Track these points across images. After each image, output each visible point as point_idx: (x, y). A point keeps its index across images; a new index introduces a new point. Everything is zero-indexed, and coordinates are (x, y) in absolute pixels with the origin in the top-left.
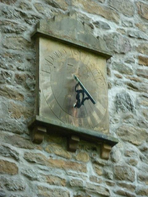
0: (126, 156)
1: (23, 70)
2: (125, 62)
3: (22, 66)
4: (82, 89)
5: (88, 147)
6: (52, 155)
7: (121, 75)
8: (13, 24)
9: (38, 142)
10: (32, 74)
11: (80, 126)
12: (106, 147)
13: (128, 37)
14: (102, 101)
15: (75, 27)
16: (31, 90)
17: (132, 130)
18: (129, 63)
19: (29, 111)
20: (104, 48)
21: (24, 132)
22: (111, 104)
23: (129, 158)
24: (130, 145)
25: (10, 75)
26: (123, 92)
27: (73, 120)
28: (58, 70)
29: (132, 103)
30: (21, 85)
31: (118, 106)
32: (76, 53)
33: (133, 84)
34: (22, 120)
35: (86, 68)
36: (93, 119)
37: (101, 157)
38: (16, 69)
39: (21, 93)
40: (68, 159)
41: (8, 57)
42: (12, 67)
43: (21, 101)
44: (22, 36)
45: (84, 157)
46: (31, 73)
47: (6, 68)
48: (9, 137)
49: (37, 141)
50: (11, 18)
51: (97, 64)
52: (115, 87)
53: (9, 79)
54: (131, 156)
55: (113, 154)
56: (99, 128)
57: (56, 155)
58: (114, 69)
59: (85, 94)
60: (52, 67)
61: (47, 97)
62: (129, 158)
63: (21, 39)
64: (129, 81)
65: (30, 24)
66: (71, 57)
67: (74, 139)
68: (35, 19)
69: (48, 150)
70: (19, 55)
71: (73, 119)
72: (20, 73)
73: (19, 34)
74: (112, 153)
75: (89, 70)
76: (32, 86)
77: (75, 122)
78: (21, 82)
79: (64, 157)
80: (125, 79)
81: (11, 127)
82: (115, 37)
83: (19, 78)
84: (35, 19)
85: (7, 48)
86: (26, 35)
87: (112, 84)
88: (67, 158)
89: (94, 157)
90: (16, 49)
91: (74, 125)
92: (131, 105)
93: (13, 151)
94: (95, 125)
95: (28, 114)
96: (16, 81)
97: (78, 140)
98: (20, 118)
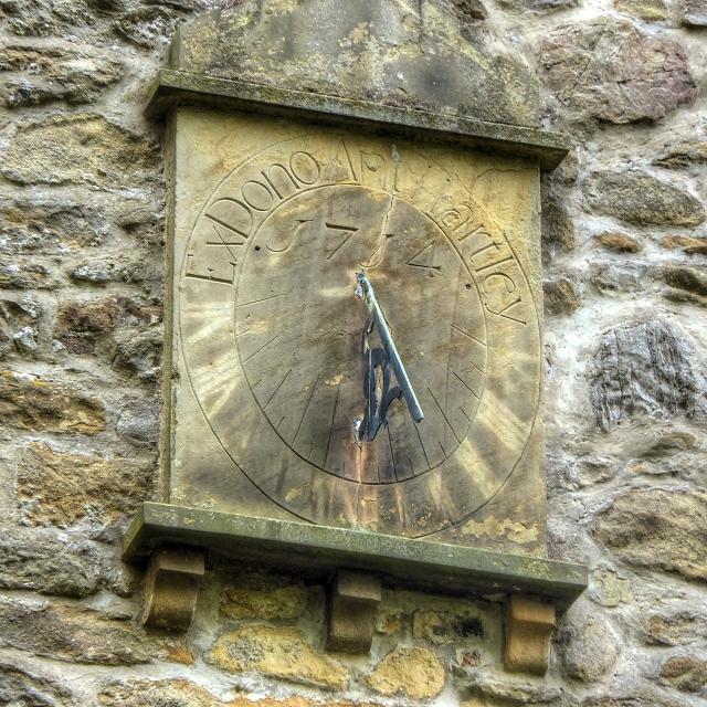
0: (648, 644)
1: (99, 284)
2: (658, 164)
3: (96, 261)
4: (382, 347)
5: (435, 621)
6: (247, 681)
7: (631, 234)
8: (50, 61)
9: (170, 628)
10: (148, 292)
11: (389, 522)
12: (525, 613)
13: (675, 34)
14: (509, 387)
15: (371, 32)
16: (140, 375)
17: (682, 512)
18: (676, 167)
19: (126, 476)
20: (529, 110)
21: (103, 584)
22: (567, 396)
23: (664, 655)
24: (672, 584)
25: (29, 314)
26: (639, 320)
27: (347, 500)
28: (274, 260)
29: (684, 374)
30: (95, 356)
31: (611, 394)
32: (373, 161)
33: (694, 271)
34: (89, 527)
35: (428, 227)
36: (459, 485)
37: (511, 668)
38: (66, 282)
39: (87, 394)
40: (333, 691)
41: (23, 228)
42: (44, 273)
43: (89, 435)
44: (98, 110)
45: (418, 672)
46: (140, 293)
47: (16, 286)
48: (22, 619)
49: (164, 622)
50: (37, 30)
51: (487, 200)
52: (597, 298)
53: (24, 332)
54: (672, 641)
55: (574, 642)
56: (489, 520)
57: (270, 677)
58: (593, 207)
59: (393, 377)
60: (243, 253)
61: (211, 400)
62: (664, 655)
63: (93, 128)
64: (671, 258)
65: (145, 47)
66: (349, 184)
67: (353, 591)
68: (162, 13)
69: (224, 657)
70: (75, 211)
71: (352, 491)
72: (85, 297)
73: (85, 102)
74: (563, 641)
75: (433, 234)
76: (144, 353)
77: (358, 508)
78: (90, 340)
79: (310, 686)
80: (657, 254)
81: (31, 568)
82: (604, 41)
83: (77, 322)
84: (166, 17)
85: (21, 184)
86: (122, 109)
87: (581, 288)
88: (328, 689)
89: (470, 670)
90: (65, 183)
91: (357, 523)
92: (679, 382)
93: (41, 682)
94: (466, 508)
95: (124, 492)
96: (62, 338)
97: (374, 595)
98: (79, 516)
